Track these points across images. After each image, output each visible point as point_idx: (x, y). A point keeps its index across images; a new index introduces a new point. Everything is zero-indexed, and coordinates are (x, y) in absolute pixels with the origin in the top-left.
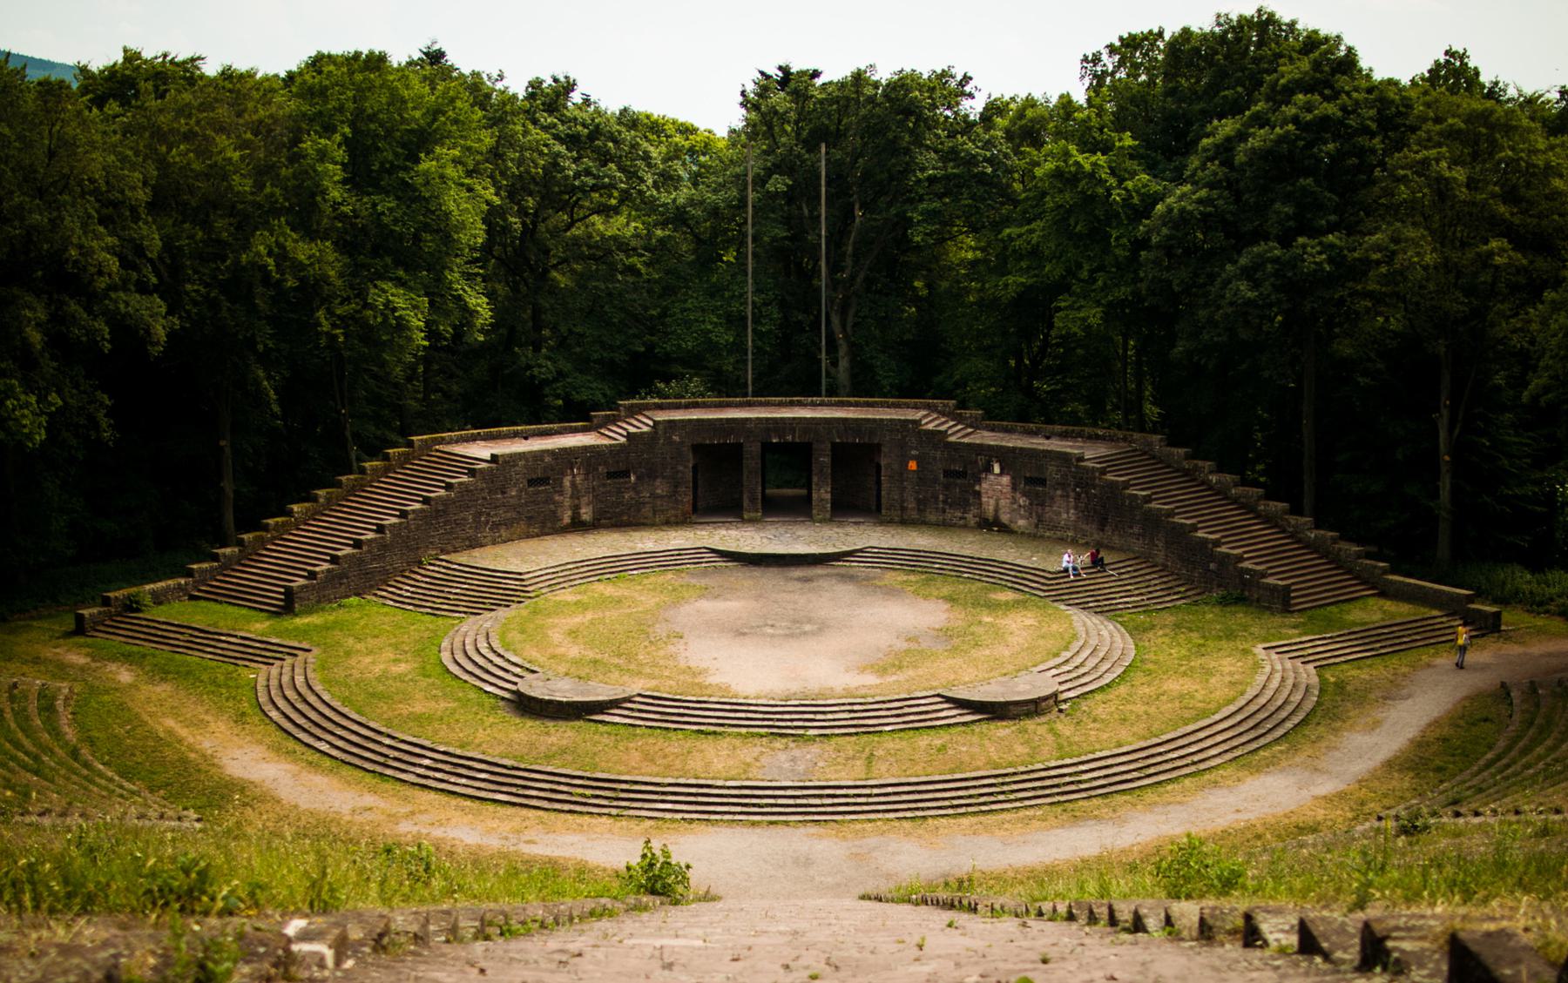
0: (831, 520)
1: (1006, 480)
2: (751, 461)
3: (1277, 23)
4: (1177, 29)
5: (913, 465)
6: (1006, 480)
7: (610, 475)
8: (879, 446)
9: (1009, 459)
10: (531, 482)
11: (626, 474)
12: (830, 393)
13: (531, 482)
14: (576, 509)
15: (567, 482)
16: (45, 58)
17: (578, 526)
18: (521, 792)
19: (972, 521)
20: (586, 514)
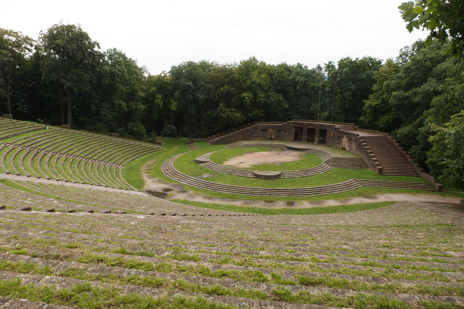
0: (293, 141)
1: (346, 139)
2: (317, 132)
3: (373, 59)
4: (170, 69)
5: (332, 134)
6: (346, 139)
7: (278, 131)
8: (326, 130)
9: (348, 135)
10: (262, 130)
11: (281, 131)
12: (319, 120)
13: (262, 130)
14: (271, 136)
15: (269, 131)
16: (226, 53)
17: (271, 139)
18: (32, 142)
19: (341, 147)
20: (273, 137)
